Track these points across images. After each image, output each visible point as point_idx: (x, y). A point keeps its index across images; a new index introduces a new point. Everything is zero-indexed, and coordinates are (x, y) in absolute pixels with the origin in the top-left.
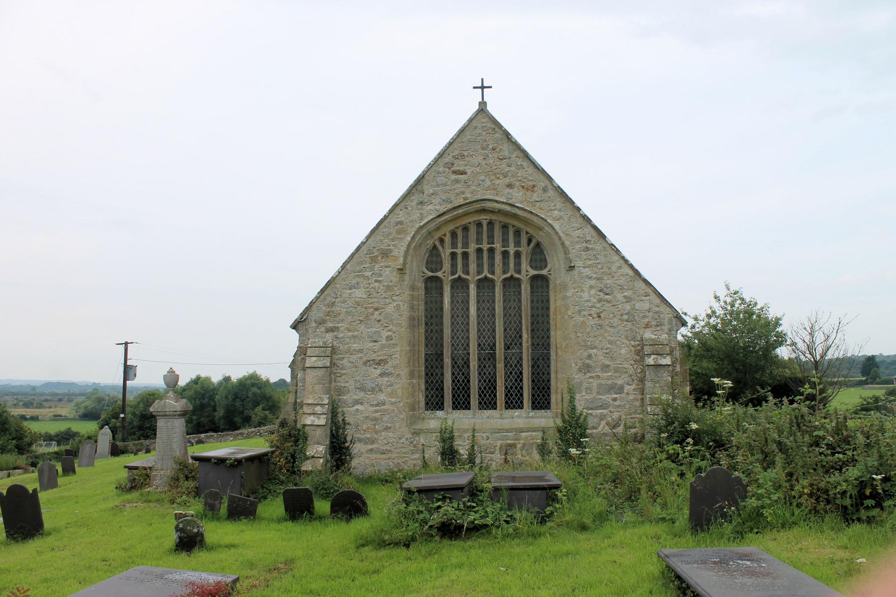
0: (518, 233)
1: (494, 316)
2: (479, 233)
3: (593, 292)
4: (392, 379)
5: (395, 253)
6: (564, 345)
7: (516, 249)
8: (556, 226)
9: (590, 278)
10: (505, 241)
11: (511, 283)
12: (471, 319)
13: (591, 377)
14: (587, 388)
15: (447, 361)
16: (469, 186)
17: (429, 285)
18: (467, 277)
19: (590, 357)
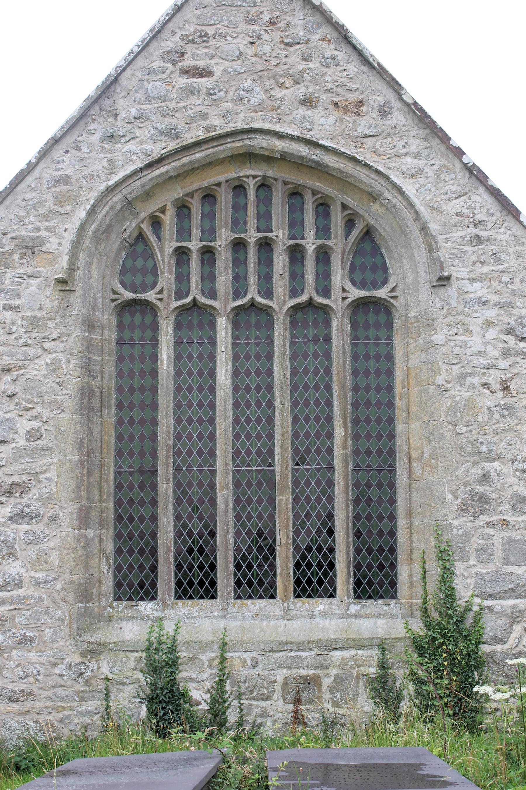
0: (323, 207)
1: (270, 388)
2: (239, 208)
3: (492, 334)
4: (38, 527)
5: (52, 245)
6: (427, 451)
7: (319, 242)
8: (410, 188)
9: (485, 303)
10: (296, 225)
11: (310, 315)
12: (220, 394)
13: (488, 524)
14: (480, 550)
15: (166, 488)
16: (217, 102)
17: (127, 318)
18: (211, 302)
19: (485, 478)
